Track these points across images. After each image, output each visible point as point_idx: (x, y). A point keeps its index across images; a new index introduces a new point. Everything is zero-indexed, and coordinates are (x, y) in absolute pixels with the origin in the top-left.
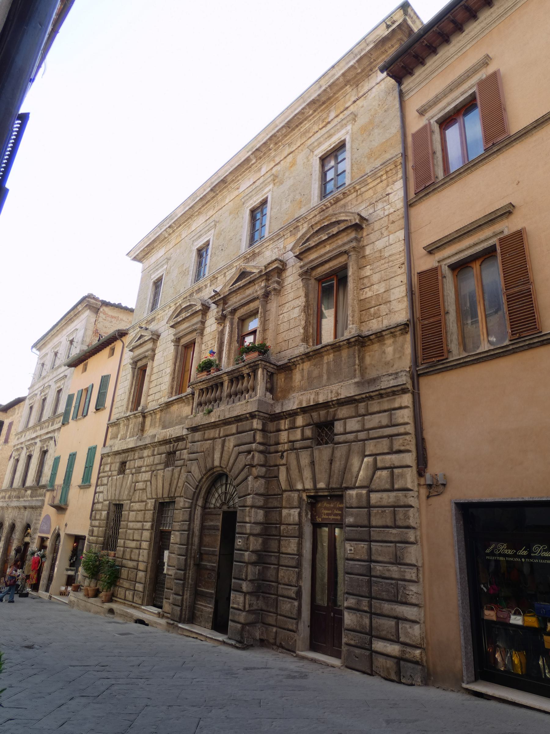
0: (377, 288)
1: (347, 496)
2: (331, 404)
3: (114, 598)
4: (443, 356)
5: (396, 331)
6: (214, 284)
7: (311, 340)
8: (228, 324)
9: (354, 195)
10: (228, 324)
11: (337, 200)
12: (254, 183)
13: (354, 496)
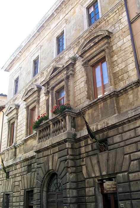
12: (57, 25)
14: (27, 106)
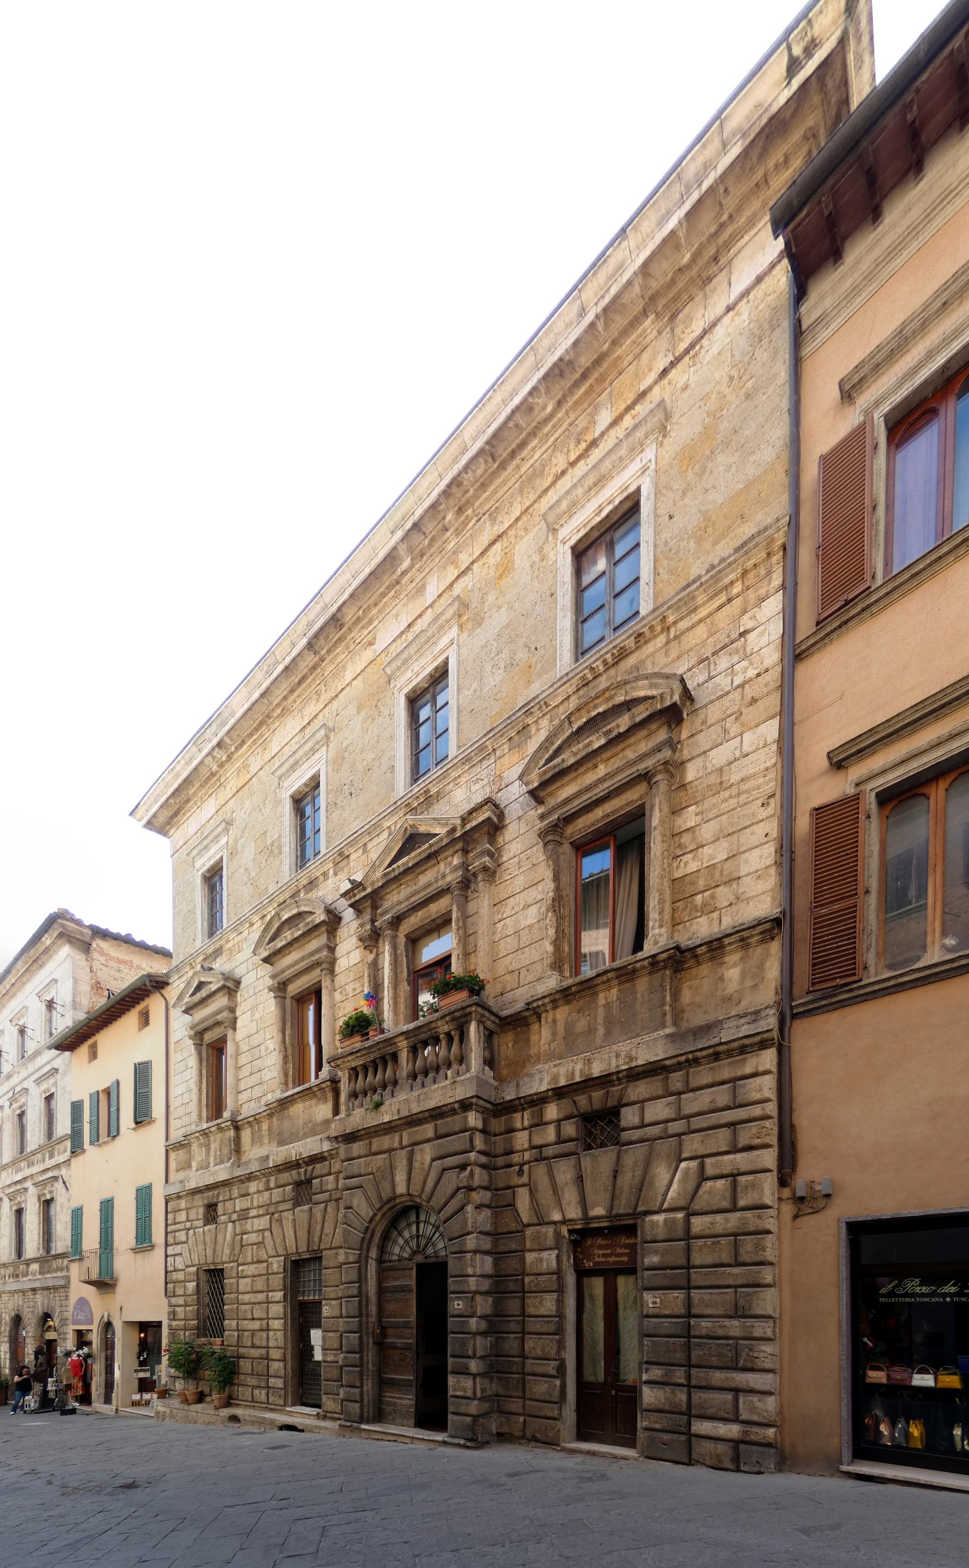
0: (711, 851)
1: (647, 1225)
2: (615, 1077)
3: (232, 1401)
4: (854, 974)
5: (752, 936)
6: (342, 869)
7: (566, 967)
8: (386, 949)
9: (662, 639)
10: (387, 948)
11: (622, 655)
12: (409, 626)
13: (661, 1223)
14: (279, 983)
